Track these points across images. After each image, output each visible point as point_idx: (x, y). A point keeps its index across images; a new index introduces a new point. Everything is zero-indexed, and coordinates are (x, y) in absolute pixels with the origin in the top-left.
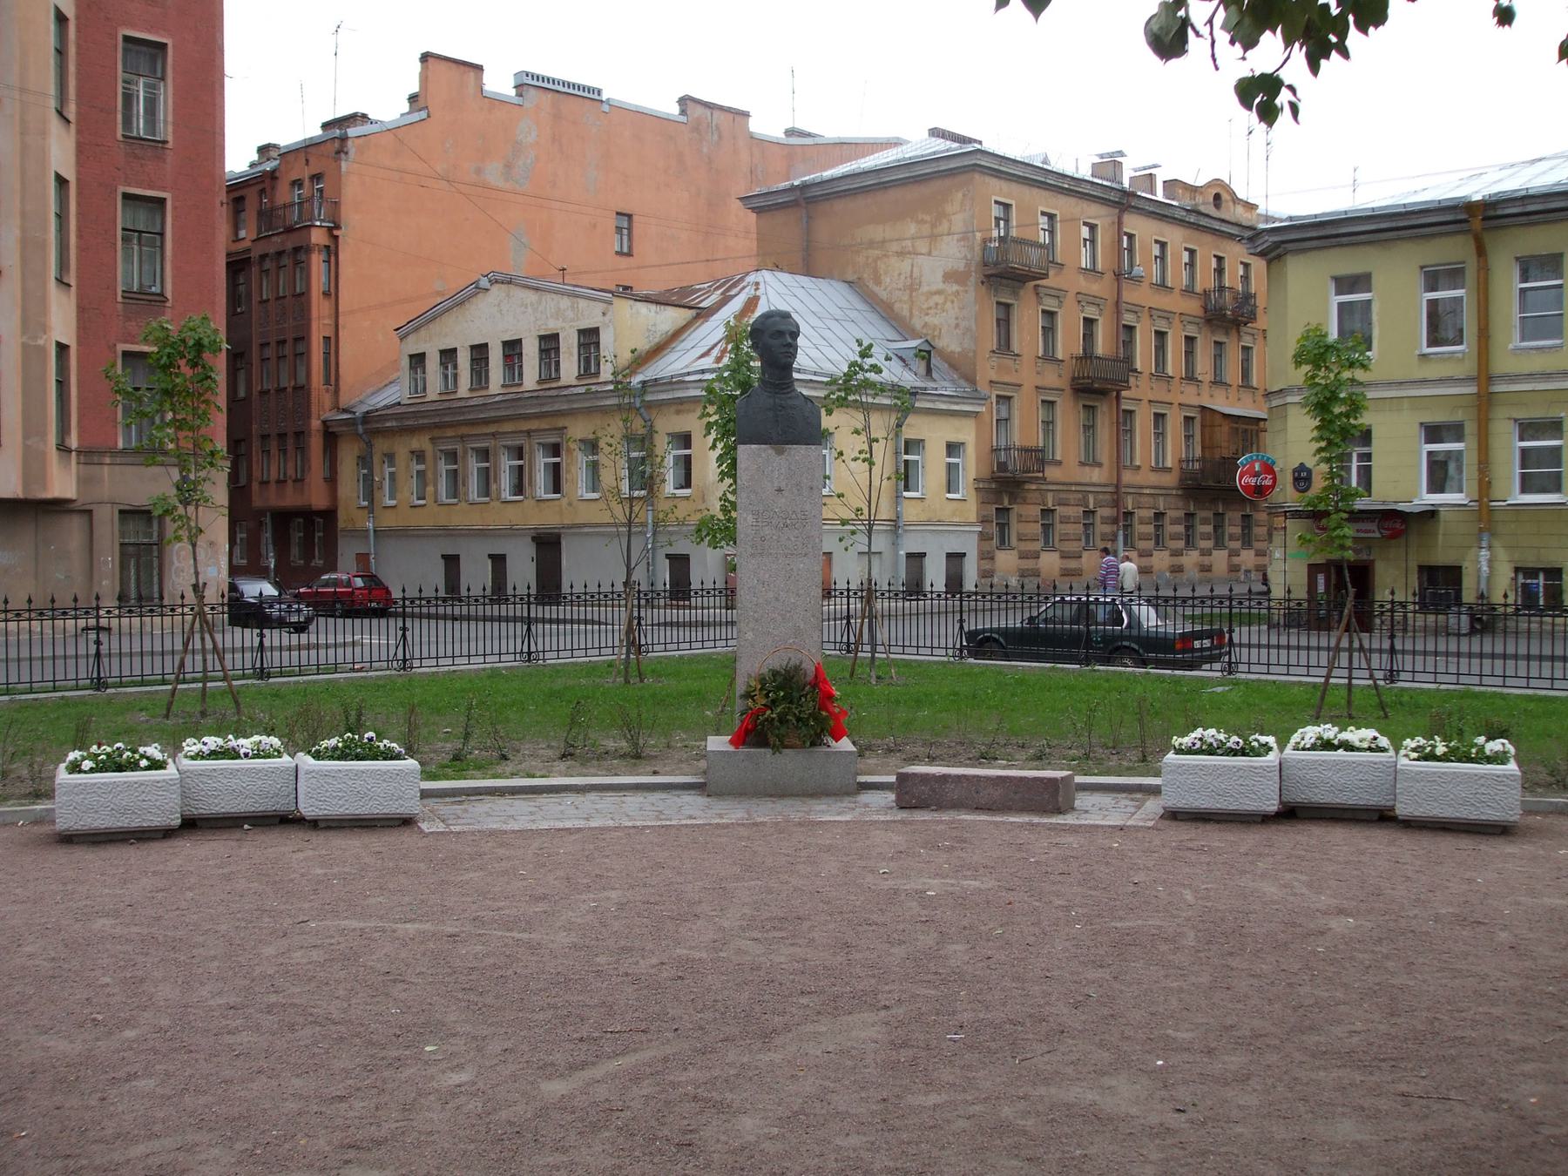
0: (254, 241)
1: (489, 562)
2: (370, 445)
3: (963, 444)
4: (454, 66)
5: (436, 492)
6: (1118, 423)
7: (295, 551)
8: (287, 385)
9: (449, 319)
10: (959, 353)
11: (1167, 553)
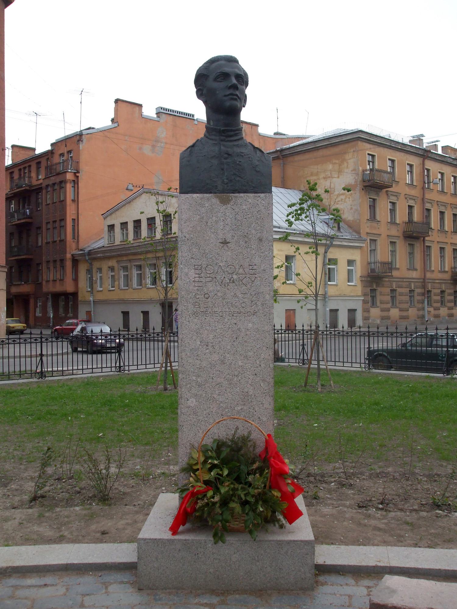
0: (43, 179)
1: (142, 314)
2: (91, 264)
3: (355, 260)
4: (130, 104)
5: (119, 284)
6: (424, 251)
7: (61, 310)
8: (57, 240)
9: (124, 210)
10: (352, 221)
11: (446, 308)
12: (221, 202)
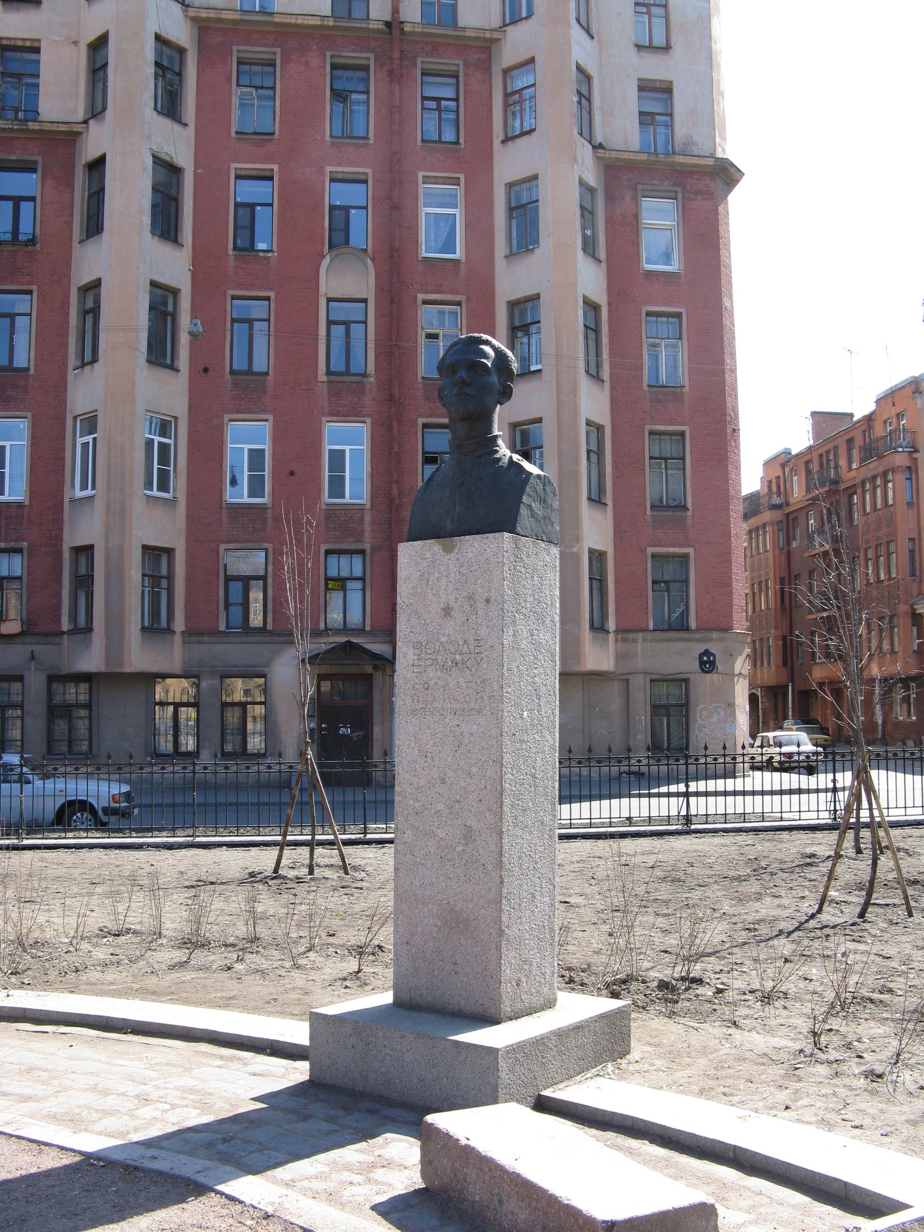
12: (444, 551)
